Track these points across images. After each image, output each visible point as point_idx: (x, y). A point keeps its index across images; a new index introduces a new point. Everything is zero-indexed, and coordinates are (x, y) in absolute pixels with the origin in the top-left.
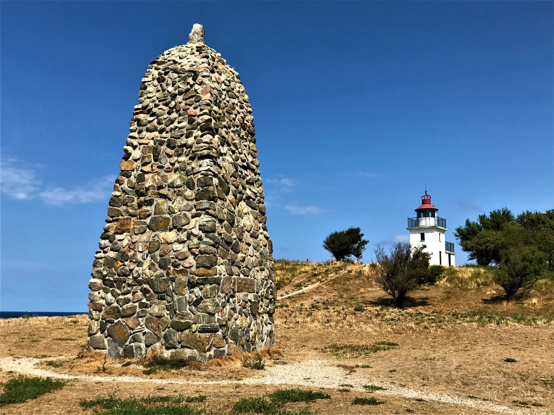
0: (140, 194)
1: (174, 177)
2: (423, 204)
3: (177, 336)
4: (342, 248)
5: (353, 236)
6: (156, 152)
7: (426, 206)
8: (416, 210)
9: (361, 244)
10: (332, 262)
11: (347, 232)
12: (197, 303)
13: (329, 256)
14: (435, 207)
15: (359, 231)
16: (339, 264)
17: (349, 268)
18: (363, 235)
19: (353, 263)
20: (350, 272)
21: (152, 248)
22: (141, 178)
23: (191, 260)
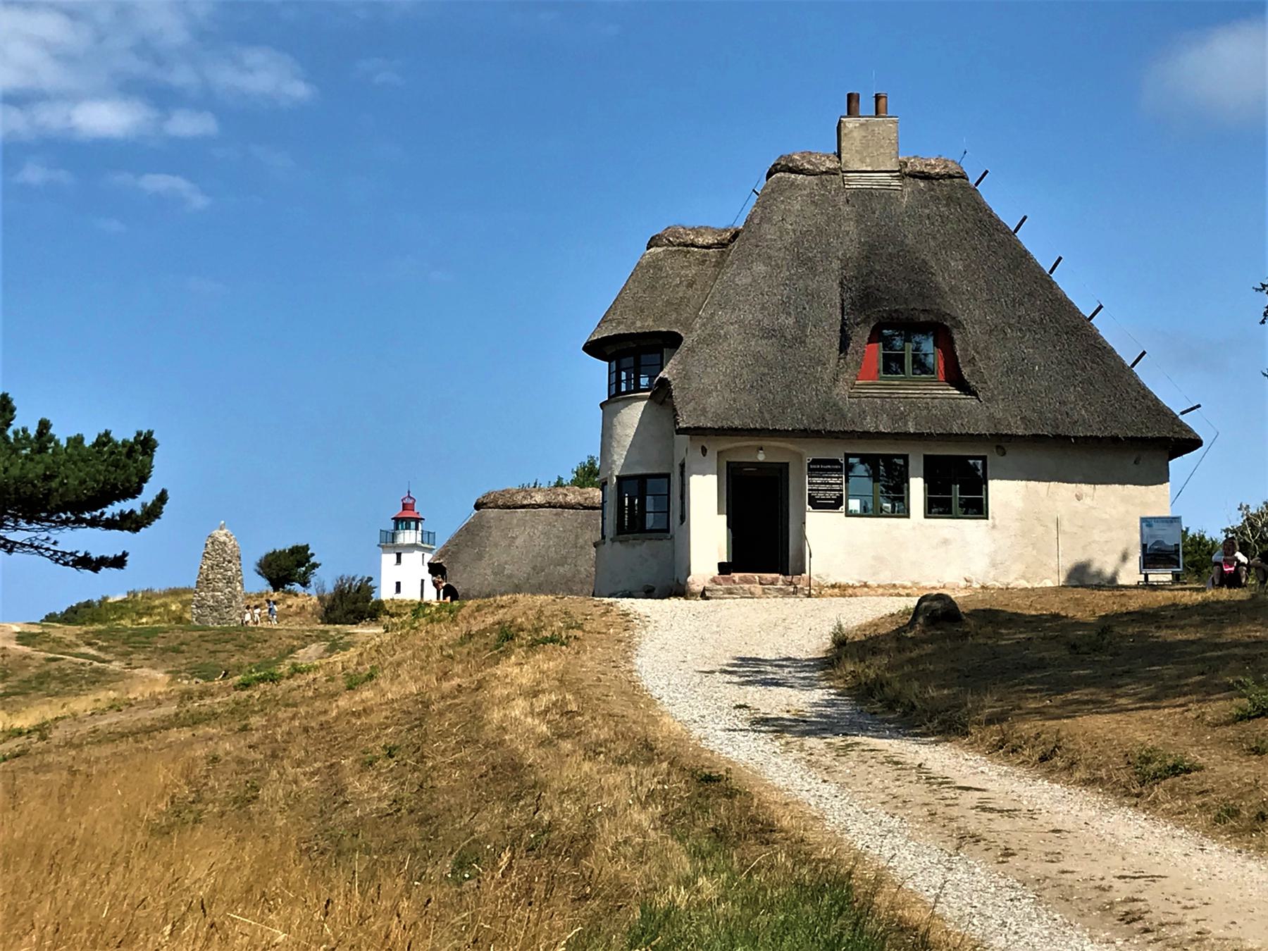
0: (207, 580)
1: (219, 576)
2: (404, 509)
3: (221, 622)
4: (281, 574)
5: (298, 557)
6: (212, 568)
7: (408, 514)
8: (393, 519)
9: (310, 568)
10: (267, 593)
11: (290, 550)
12: (227, 613)
13: (262, 584)
14: (421, 516)
15: (308, 549)
16: (276, 596)
17: (289, 602)
18: (313, 555)
19: (296, 595)
20: (290, 607)
21: (213, 597)
22: (207, 575)
23: (226, 601)
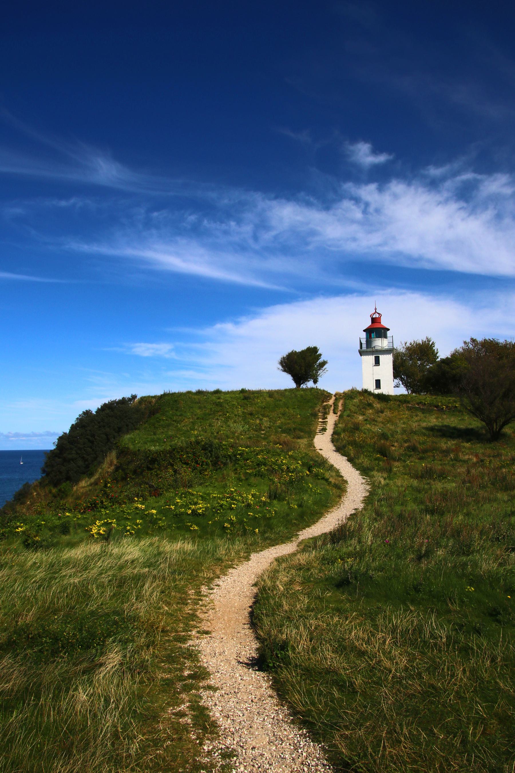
8: (364, 331)
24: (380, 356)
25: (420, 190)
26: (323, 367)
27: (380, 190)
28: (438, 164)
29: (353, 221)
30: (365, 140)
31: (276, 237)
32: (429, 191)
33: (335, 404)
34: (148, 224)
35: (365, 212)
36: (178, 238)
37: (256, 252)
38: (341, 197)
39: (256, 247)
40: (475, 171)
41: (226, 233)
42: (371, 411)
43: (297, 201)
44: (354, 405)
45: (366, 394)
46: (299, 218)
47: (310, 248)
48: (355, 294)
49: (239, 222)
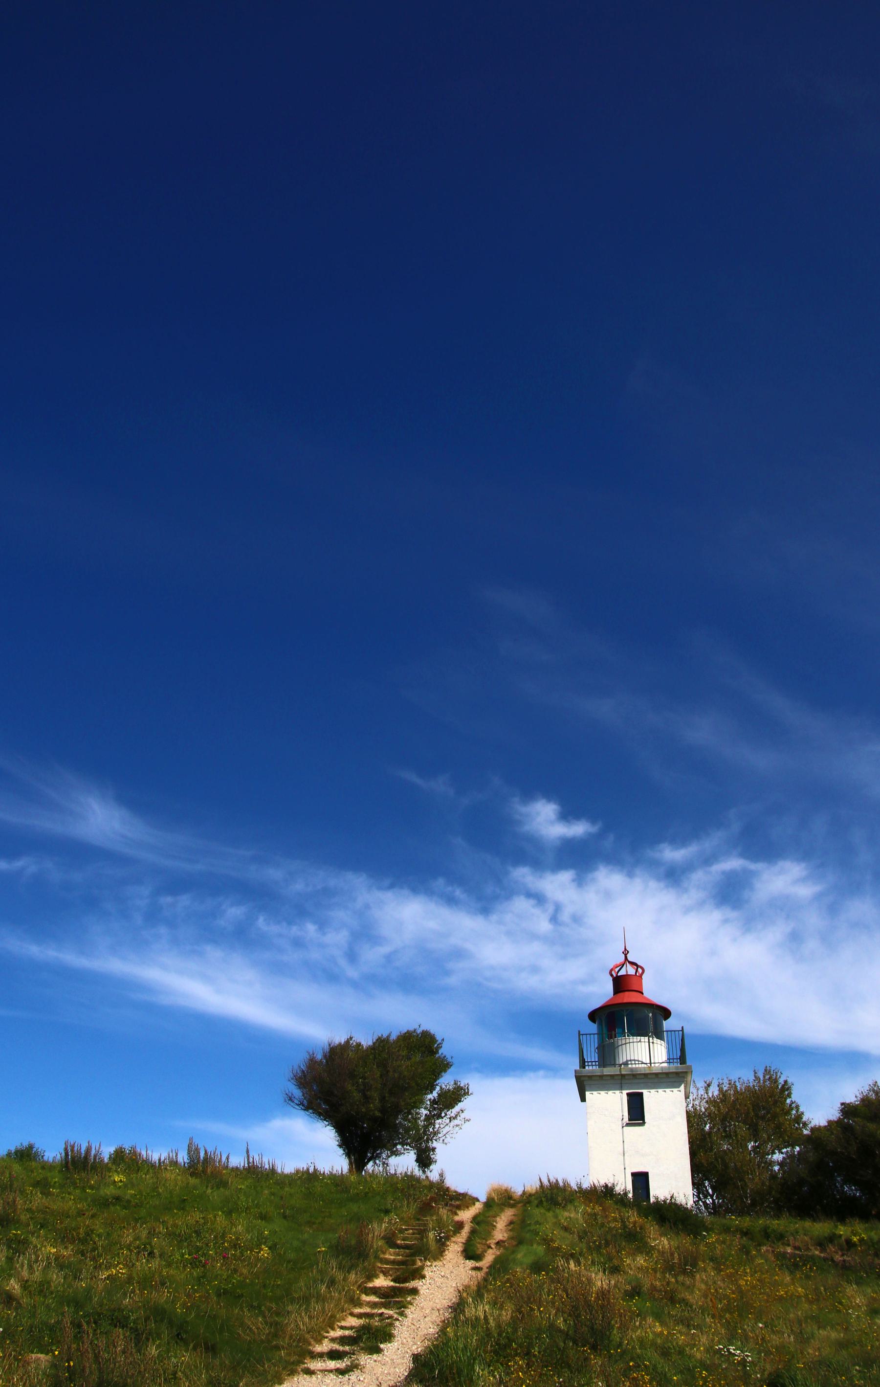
24: (646, 1093)
25: (653, 884)
26: (451, 1106)
27: (580, 881)
28: (679, 841)
29: (534, 936)
30: (549, 795)
31: (389, 958)
32: (667, 887)
33: (483, 1223)
34: (153, 916)
35: (554, 919)
36: (209, 948)
37: (355, 985)
38: (509, 892)
39: (352, 973)
40: (744, 855)
41: (298, 943)
42: (641, 1260)
43: (430, 893)
44: (566, 1229)
45: (609, 1202)
46: (432, 924)
47: (452, 981)
48: (541, 1073)
49: (323, 925)
